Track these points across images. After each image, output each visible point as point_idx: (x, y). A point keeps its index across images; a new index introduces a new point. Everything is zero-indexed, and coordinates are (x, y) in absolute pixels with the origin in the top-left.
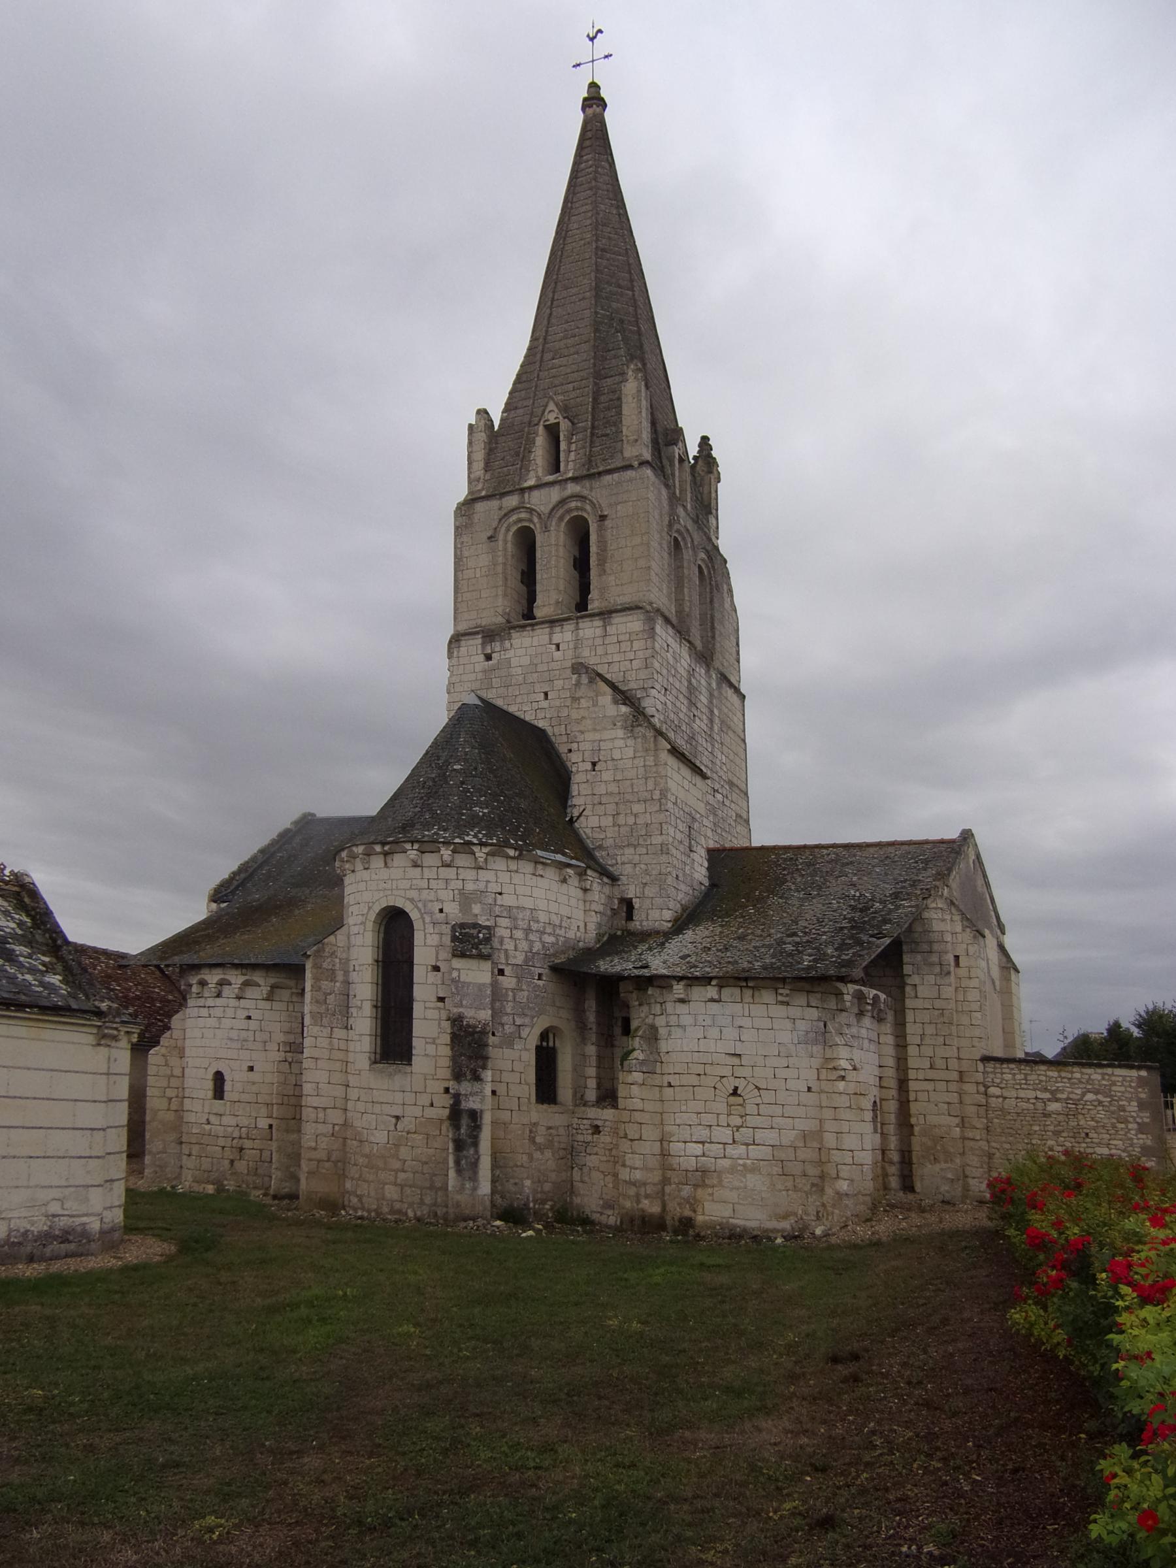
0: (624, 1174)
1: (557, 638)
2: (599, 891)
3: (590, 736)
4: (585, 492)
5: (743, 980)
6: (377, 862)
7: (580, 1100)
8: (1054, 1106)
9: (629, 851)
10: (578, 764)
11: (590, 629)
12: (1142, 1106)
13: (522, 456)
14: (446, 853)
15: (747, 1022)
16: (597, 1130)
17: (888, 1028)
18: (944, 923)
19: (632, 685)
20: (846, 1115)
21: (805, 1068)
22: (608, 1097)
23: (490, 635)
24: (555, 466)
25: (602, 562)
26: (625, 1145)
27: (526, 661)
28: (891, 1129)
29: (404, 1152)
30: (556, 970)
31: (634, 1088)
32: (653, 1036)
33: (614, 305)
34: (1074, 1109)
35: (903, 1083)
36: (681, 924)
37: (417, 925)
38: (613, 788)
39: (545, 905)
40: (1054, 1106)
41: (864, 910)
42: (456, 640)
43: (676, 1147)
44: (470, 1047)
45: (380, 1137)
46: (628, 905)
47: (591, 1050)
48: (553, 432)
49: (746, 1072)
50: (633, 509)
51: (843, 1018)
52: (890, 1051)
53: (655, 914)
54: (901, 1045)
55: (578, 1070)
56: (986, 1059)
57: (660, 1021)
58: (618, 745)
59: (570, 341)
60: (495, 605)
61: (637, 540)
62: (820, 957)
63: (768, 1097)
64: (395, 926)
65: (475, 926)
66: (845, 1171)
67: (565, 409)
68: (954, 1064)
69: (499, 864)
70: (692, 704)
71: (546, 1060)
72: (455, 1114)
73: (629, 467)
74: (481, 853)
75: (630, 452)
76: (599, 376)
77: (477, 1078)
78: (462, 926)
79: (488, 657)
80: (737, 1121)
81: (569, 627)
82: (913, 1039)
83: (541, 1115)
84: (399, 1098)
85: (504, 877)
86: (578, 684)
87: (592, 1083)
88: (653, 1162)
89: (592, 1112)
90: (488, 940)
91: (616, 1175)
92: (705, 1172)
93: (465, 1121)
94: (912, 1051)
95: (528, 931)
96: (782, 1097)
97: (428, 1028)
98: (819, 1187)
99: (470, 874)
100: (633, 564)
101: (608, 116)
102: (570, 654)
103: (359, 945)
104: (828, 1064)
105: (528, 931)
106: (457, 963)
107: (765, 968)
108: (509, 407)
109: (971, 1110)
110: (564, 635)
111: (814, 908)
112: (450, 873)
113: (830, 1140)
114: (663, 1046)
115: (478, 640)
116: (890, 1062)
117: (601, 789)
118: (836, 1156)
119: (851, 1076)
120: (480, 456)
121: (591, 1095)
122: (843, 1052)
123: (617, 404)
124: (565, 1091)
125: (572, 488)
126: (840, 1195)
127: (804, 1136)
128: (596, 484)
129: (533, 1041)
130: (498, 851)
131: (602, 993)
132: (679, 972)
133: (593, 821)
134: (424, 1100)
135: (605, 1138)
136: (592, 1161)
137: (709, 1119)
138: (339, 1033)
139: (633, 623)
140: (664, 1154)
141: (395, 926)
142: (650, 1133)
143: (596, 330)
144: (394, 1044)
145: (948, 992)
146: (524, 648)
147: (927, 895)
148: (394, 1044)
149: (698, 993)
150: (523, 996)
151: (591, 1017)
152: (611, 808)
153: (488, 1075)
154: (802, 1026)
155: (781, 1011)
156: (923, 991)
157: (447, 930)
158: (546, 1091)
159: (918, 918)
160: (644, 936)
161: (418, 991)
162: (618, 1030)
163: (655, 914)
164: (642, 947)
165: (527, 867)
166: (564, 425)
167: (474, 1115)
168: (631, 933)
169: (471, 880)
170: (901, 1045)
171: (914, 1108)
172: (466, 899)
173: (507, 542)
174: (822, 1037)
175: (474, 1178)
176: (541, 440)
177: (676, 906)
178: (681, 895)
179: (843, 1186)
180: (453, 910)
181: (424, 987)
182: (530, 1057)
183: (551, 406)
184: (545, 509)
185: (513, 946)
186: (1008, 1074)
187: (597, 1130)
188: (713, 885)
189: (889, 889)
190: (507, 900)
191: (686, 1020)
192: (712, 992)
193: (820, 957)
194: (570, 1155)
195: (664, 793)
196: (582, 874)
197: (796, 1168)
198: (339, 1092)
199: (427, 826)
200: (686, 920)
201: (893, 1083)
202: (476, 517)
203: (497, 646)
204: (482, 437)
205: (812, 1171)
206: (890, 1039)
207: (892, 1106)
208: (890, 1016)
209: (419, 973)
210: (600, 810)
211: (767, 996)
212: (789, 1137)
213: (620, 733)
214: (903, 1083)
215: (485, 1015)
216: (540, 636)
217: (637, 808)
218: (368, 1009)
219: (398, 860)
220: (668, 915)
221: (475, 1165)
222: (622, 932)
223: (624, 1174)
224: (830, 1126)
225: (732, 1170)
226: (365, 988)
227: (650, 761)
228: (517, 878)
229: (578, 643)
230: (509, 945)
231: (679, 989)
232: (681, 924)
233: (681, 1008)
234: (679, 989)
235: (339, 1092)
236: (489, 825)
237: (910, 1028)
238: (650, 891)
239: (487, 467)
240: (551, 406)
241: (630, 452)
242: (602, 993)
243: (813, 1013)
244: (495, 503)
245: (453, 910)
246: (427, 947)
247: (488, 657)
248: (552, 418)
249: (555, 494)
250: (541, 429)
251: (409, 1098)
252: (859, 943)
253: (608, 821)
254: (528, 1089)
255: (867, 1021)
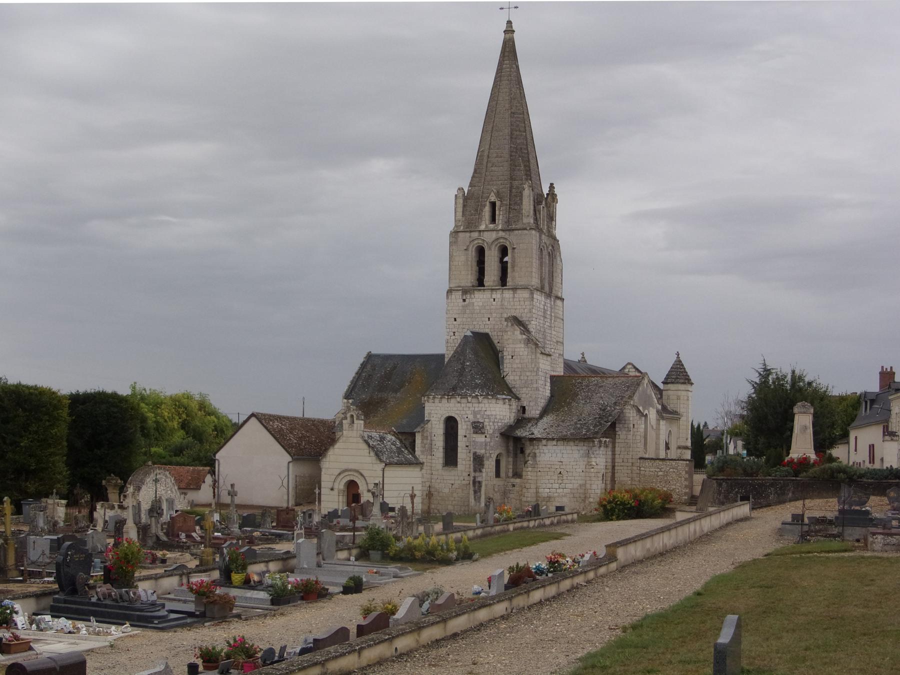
0: (524, 499)
1: (494, 296)
2: (514, 403)
3: (511, 346)
4: (507, 236)
5: (564, 439)
6: (444, 401)
7: (507, 477)
8: (660, 473)
9: (525, 389)
10: (507, 355)
11: (508, 294)
12: (686, 472)
13: (479, 211)
14: (470, 399)
15: (565, 452)
16: (514, 486)
17: (610, 449)
18: (630, 414)
19: (524, 319)
20: (593, 479)
21: (582, 465)
22: (517, 474)
23: (465, 291)
24: (493, 220)
25: (513, 267)
26: (525, 490)
27: (481, 304)
28: (608, 482)
29: (455, 495)
30: (502, 434)
31: (529, 473)
32: (535, 456)
33: (518, 141)
34: (667, 474)
35: (613, 467)
36: (541, 416)
37: (459, 422)
38: (519, 366)
39: (499, 412)
40: (660, 473)
41: (604, 410)
42: (450, 291)
43: (540, 490)
44: (478, 461)
45: (446, 491)
46: (524, 408)
47: (511, 459)
48: (493, 205)
49: (564, 467)
50: (526, 246)
51: (594, 449)
52: (610, 457)
53: (533, 412)
54: (614, 454)
55: (507, 468)
56: (641, 458)
57: (537, 451)
58: (522, 350)
59: (500, 159)
60: (468, 278)
61: (528, 260)
62: (588, 430)
63: (570, 474)
64: (451, 424)
65: (478, 422)
66: (592, 496)
67: (498, 195)
68: (630, 461)
69: (486, 401)
70: (545, 317)
71: (498, 462)
72: (474, 482)
73: (525, 229)
74: (480, 398)
75: (525, 220)
76: (512, 179)
77: (481, 471)
78: (474, 422)
79: (464, 300)
80: (560, 481)
81: (499, 292)
82: (617, 452)
83: (497, 482)
84: (453, 478)
85: (487, 405)
86: (507, 326)
87: (511, 471)
88: (534, 495)
89: (512, 480)
90: (483, 427)
91: (521, 500)
92: (550, 497)
93: (477, 484)
94: (617, 456)
95: (494, 422)
96: (574, 474)
97: (463, 455)
98: (584, 501)
99: (476, 405)
100: (526, 270)
101: (515, 35)
102: (499, 303)
103: (437, 430)
104: (589, 464)
105: (494, 422)
106: (475, 436)
107: (571, 434)
108: (471, 185)
109: (635, 475)
110: (497, 295)
111: (587, 409)
112: (470, 405)
113: (588, 486)
114: (538, 459)
115: (460, 293)
116: (610, 460)
117: (515, 366)
118: (590, 491)
119: (596, 467)
120: (460, 210)
121: (510, 474)
122: (594, 460)
123: (520, 195)
124: (503, 474)
125: (501, 234)
126: (590, 503)
127: (580, 485)
128: (512, 233)
129: (494, 459)
130: (486, 397)
131: (516, 442)
132: (544, 436)
133: (512, 378)
134: (462, 478)
135: (516, 488)
136: (512, 496)
137: (552, 481)
138: (429, 457)
139: (525, 294)
140: (537, 492)
141: (451, 424)
142: (533, 486)
143: (511, 156)
144: (451, 459)
145: (630, 437)
146: (480, 298)
147: (626, 403)
148: (451, 459)
149: (550, 443)
150: (492, 444)
151: (511, 448)
152: (519, 374)
153: (484, 470)
154: (582, 452)
155: (575, 448)
156: (621, 437)
157: (469, 424)
158: (498, 475)
159: (622, 412)
160: (530, 420)
161: (459, 444)
162: (519, 452)
163: (533, 412)
164: (530, 425)
165: (494, 401)
166: (498, 203)
167: (479, 482)
168: (525, 419)
169: (477, 407)
170: (614, 454)
171: (616, 475)
172: (475, 413)
173: (472, 254)
174: (588, 455)
175: (479, 502)
176: (487, 210)
177: (540, 408)
178: (542, 403)
179: (591, 500)
180: (471, 417)
181: (461, 443)
182: (494, 463)
183: (492, 194)
184: (490, 241)
185: (490, 428)
186: (647, 463)
187: (514, 486)
188: (552, 396)
189: (613, 400)
190: (488, 413)
191: (546, 451)
192: (554, 442)
193: (588, 430)
194: (505, 494)
195: (538, 369)
196: (510, 400)
197: (577, 495)
198: (429, 476)
199: (462, 388)
200: (545, 412)
201: (610, 467)
202: (459, 239)
203: (468, 296)
204: (461, 201)
205: (582, 496)
206: (610, 453)
207: (610, 475)
208: (610, 445)
209: (460, 438)
210: (514, 373)
211: (572, 443)
212: (576, 486)
213: (523, 346)
214: (613, 467)
215: (483, 451)
216: (487, 294)
217: (528, 374)
218: (441, 450)
219: (453, 400)
220: (538, 412)
221: (480, 497)
222: (522, 420)
223: (524, 499)
224: (588, 482)
225: (558, 496)
226: (439, 442)
227: (533, 357)
228: (491, 405)
229: (503, 299)
230: (488, 428)
231: (544, 442)
232: (541, 416)
233: (544, 448)
234: (544, 442)
235: (429, 476)
236: (481, 387)
237: (617, 449)
238: (532, 404)
239: (463, 215)
240: (492, 194)
241: (525, 220)
242: (516, 442)
243: (585, 448)
244: (468, 234)
245: (471, 417)
246: (463, 429)
247: (464, 300)
248: (493, 198)
249: (494, 235)
250: (488, 203)
251: (457, 478)
252: (601, 424)
253: (517, 378)
254: (493, 474)
255: (602, 449)
